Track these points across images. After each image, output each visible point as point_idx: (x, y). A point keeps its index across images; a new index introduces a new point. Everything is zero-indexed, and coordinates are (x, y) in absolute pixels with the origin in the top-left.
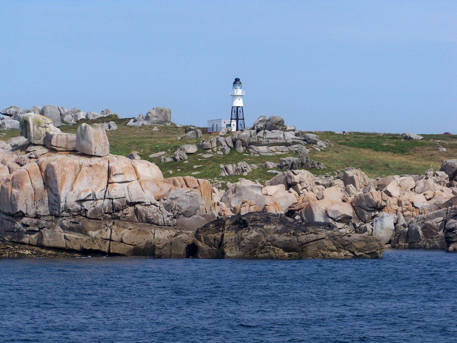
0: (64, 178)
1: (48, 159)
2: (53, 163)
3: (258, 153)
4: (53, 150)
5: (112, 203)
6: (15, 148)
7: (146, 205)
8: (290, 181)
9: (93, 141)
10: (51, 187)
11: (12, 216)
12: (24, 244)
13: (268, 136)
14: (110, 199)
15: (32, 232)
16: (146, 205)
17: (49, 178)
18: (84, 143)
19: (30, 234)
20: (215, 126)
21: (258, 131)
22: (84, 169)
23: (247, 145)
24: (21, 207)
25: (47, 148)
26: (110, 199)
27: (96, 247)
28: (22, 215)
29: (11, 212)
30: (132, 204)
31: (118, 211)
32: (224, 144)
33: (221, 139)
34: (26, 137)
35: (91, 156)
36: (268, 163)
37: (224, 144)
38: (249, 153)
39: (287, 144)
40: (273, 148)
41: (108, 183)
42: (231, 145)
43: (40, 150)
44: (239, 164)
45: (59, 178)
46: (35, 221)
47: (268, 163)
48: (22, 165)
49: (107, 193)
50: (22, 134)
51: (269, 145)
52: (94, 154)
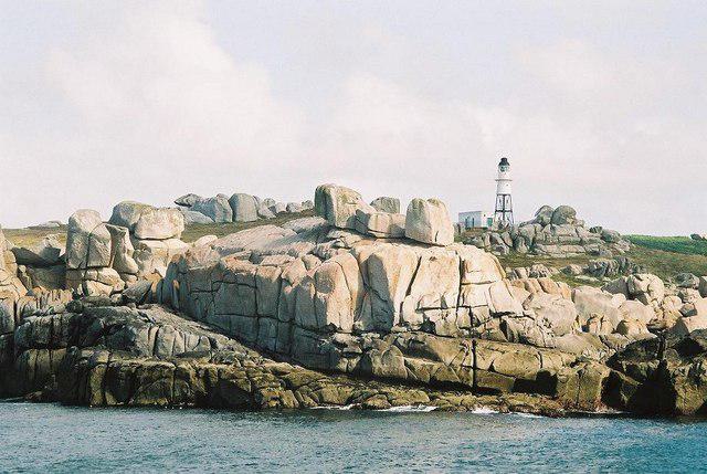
0: (397, 276)
1: (366, 249)
2: (379, 255)
3: (548, 254)
4: (369, 236)
5: (471, 314)
6: (304, 235)
7: (516, 317)
8: (632, 289)
9: (432, 222)
10: (375, 288)
11: (316, 330)
12: (340, 372)
13: (558, 233)
14: (466, 307)
15: (352, 355)
16: (516, 317)
17: (370, 273)
18: (419, 225)
19: (348, 358)
20: (471, 220)
21: (544, 225)
22: (424, 262)
23: (533, 244)
24: (332, 318)
25: (358, 233)
26: (466, 307)
27: (454, 378)
28: (334, 329)
29: (314, 325)
30: (497, 315)
31: (478, 324)
32: (500, 241)
33: (496, 236)
34: (326, 218)
35: (429, 245)
36: (573, 266)
37: (500, 241)
38: (535, 253)
39: (581, 243)
40: (565, 248)
41: (461, 284)
42: (510, 243)
43: (351, 238)
44: (535, 267)
45: (390, 276)
46: (355, 339)
47: (573, 266)
48: (323, 259)
49: (461, 300)
50: (318, 214)
51: (559, 243)
52: (434, 242)
